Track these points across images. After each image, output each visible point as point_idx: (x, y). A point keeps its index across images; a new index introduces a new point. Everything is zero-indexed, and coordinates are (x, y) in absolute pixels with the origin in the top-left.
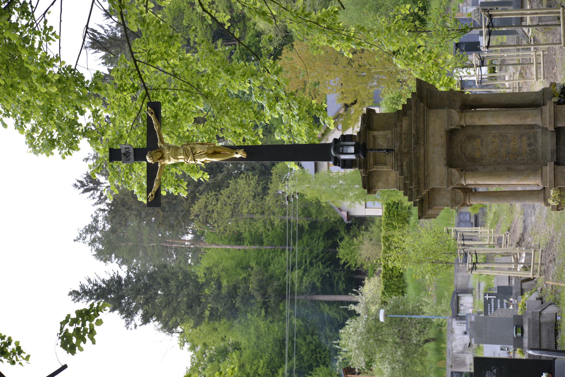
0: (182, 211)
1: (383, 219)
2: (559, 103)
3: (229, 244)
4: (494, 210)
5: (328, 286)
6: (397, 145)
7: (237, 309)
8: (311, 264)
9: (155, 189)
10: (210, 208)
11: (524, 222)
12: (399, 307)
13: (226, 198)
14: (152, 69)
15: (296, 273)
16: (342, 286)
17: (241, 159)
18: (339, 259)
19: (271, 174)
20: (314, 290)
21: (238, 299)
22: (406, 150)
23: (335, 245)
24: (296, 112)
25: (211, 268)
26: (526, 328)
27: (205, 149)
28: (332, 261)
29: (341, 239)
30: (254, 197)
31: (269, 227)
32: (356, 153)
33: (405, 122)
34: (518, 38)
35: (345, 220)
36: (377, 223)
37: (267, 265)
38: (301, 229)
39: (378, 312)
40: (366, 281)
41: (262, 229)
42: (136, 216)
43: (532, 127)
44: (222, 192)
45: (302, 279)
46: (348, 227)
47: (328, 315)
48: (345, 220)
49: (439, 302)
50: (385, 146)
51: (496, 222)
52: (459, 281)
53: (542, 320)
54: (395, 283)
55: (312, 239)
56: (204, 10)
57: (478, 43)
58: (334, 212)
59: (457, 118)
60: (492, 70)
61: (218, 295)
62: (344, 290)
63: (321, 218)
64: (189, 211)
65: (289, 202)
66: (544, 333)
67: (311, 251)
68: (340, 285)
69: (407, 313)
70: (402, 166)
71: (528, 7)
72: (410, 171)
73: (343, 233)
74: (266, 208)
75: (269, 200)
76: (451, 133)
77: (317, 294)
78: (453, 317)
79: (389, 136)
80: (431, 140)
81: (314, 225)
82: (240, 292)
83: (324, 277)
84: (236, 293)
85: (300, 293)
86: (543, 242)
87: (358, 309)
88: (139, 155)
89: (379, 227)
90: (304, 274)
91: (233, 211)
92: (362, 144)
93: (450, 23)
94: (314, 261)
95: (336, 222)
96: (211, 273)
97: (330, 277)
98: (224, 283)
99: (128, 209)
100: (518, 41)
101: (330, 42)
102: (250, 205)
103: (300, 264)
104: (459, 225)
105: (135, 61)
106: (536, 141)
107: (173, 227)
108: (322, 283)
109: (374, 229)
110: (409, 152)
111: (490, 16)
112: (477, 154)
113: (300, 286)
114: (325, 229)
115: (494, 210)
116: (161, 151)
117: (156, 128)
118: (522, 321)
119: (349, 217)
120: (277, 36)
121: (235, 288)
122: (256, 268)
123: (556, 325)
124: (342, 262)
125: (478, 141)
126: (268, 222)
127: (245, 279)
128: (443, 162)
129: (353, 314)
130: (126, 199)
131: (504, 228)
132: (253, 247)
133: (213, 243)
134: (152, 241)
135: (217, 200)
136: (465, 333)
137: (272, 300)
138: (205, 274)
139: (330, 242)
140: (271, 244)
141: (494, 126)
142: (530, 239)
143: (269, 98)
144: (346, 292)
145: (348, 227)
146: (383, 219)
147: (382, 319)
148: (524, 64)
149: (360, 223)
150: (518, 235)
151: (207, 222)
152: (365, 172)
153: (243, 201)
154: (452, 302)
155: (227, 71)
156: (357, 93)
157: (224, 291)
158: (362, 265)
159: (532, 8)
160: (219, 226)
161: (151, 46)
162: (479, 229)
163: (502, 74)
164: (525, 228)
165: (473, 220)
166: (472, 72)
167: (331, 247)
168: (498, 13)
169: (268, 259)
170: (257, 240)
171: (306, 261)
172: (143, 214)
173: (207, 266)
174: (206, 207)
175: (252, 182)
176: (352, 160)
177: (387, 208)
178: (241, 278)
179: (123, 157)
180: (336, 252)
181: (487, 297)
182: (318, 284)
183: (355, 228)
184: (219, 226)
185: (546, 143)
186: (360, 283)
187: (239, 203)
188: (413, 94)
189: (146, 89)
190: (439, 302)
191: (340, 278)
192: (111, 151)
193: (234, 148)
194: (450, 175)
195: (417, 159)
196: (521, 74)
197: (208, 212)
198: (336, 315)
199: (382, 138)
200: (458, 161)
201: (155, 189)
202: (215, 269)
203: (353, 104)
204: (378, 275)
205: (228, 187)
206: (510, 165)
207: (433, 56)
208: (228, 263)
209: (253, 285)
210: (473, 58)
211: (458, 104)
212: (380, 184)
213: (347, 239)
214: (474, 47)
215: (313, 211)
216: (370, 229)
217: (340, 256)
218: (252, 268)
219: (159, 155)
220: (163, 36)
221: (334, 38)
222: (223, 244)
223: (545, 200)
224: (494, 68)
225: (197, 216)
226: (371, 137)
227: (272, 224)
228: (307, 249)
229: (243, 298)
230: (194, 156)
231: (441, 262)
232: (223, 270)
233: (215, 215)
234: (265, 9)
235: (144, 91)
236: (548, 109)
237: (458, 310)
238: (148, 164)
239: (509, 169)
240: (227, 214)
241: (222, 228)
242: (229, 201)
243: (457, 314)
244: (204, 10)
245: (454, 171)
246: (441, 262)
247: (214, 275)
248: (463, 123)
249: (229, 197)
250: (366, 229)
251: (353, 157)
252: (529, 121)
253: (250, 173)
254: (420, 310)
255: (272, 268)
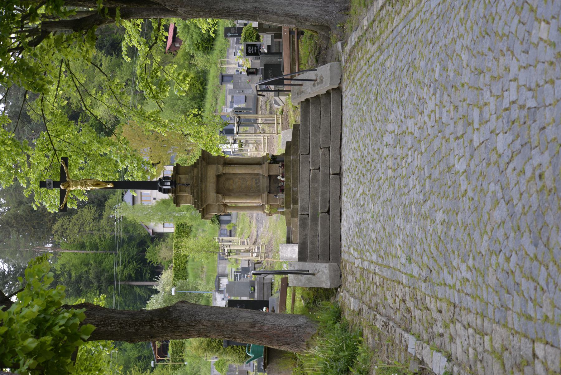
0: (47, 228)
1: (174, 234)
2: (270, 163)
3: (76, 250)
4: (241, 227)
5: (139, 276)
6: (192, 182)
7: (81, 291)
8: (129, 262)
9: (64, 203)
10: (65, 227)
11: (257, 232)
12: (183, 287)
13: (75, 221)
14: (58, 140)
15: (119, 269)
16: (148, 276)
17: (111, 188)
18: (147, 259)
19: (105, 206)
20: (130, 278)
21: (82, 284)
22: (196, 185)
23: (144, 251)
24: (135, 165)
25: (65, 264)
26: (256, 288)
27: (92, 182)
28: (143, 261)
29: (148, 247)
30: (94, 220)
31: (103, 239)
32: (171, 185)
33: (196, 171)
34: (255, 129)
35: (151, 234)
36: (171, 236)
37: (101, 262)
38: (123, 240)
39: (171, 290)
40: (163, 272)
41: (98, 240)
42: (16, 231)
43: (258, 174)
44: (73, 217)
45: (123, 271)
46: (152, 240)
47: (139, 294)
48: (151, 234)
49: (208, 283)
50: (185, 182)
51: (242, 234)
52: (220, 270)
53: (265, 282)
54: (181, 273)
55: (130, 247)
56: (87, 109)
57: (233, 130)
58: (144, 230)
59: (221, 170)
60: (241, 146)
61: (69, 281)
62: (149, 278)
63: (135, 234)
64: (51, 229)
65: (117, 223)
66: (265, 289)
67: (129, 254)
68: (147, 275)
69: (188, 290)
70: (194, 193)
71: (260, 113)
72: (198, 195)
73: (149, 243)
74: (101, 227)
75: (103, 222)
76: (218, 177)
77: (133, 281)
78: (216, 291)
79: (187, 177)
80: (208, 180)
81: (131, 239)
82: (83, 280)
83: (137, 270)
84: (81, 280)
85: (122, 281)
86: (266, 241)
87: (159, 289)
88: (56, 185)
89: (172, 239)
90: (124, 268)
91: (80, 228)
92: (174, 181)
93: (217, 120)
94: (131, 260)
95: (144, 237)
96: (65, 268)
97: (141, 270)
98: (73, 274)
99: (11, 227)
100: (255, 131)
101: (155, 128)
102: (91, 225)
103: (122, 262)
104: (220, 236)
105: (49, 135)
106: (259, 181)
107: (40, 238)
108: (135, 274)
109: (169, 240)
110: (197, 186)
111: (239, 117)
112: (231, 187)
113: (122, 276)
114: (138, 241)
115: (241, 227)
116: (68, 183)
117: (66, 171)
118: (254, 284)
119: (154, 233)
120: (110, 120)
121: (80, 277)
122: (94, 265)
123: (272, 284)
124: (148, 261)
125: (232, 181)
126: (102, 236)
127: (86, 271)
128: (214, 191)
129: (156, 292)
130: (10, 220)
131: (246, 236)
132: (92, 252)
133: (66, 249)
134: (26, 248)
135: (70, 222)
136: (223, 299)
137: (104, 284)
138: (61, 268)
139: (141, 249)
140: (104, 249)
141: (239, 174)
142: (260, 241)
143: (121, 157)
144: (151, 280)
145: (152, 240)
146: (174, 234)
147: (173, 294)
148: (258, 143)
149: (161, 236)
150: (254, 240)
151: (63, 236)
152: (175, 195)
153: (86, 223)
154: (215, 282)
155: (99, 142)
156: (161, 157)
157: (73, 279)
158: (160, 263)
159: (262, 114)
160: (70, 238)
161: (58, 127)
162: (232, 238)
163: (246, 148)
164: (257, 235)
165: (228, 234)
166: (229, 147)
167: (141, 252)
168: (243, 117)
169: (102, 259)
170: (95, 247)
171: (126, 261)
172: (21, 230)
173: (62, 263)
174: (62, 226)
175: (92, 210)
176: (168, 189)
177: (177, 227)
178: (84, 270)
179: (47, 186)
180: (145, 255)
181: (236, 273)
182: (133, 275)
183: (157, 240)
184: (70, 238)
185: (264, 183)
186: (160, 273)
187: (84, 224)
188: (200, 157)
189: (55, 150)
190: (208, 283)
191: (147, 271)
192: (41, 182)
193: (108, 182)
194: (217, 197)
195: (201, 189)
196: (256, 148)
197: (64, 229)
198: (144, 294)
199: (184, 178)
200: (222, 191)
201: (64, 203)
202: (67, 265)
203: (158, 163)
204: (171, 268)
205: (77, 214)
206: (247, 193)
207: (210, 136)
208: (76, 262)
209: (92, 275)
210: (230, 138)
211: (222, 163)
212: (182, 202)
213: (151, 246)
214: (230, 132)
215: (131, 229)
216: (166, 241)
217: (147, 258)
218: (91, 265)
219: (67, 185)
220: (64, 122)
221: (157, 126)
222: (72, 250)
223: (263, 210)
224: (242, 145)
225: (56, 231)
226: (179, 179)
227: (104, 236)
228: (127, 253)
229: (85, 283)
230: (86, 186)
231: (211, 252)
232: (72, 266)
233: (68, 231)
234: (120, 109)
235: (53, 151)
236: (265, 166)
237: (219, 287)
238: (61, 190)
239: (246, 195)
240: (76, 231)
241: (72, 239)
242: (77, 222)
243: (218, 290)
244: (87, 109)
245: (219, 195)
246: (211, 252)
247: (67, 269)
248: (224, 172)
249: (77, 220)
250: (164, 241)
251: (169, 187)
252: (256, 172)
253: (91, 205)
254: (196, 288)
255: (104, 264)
